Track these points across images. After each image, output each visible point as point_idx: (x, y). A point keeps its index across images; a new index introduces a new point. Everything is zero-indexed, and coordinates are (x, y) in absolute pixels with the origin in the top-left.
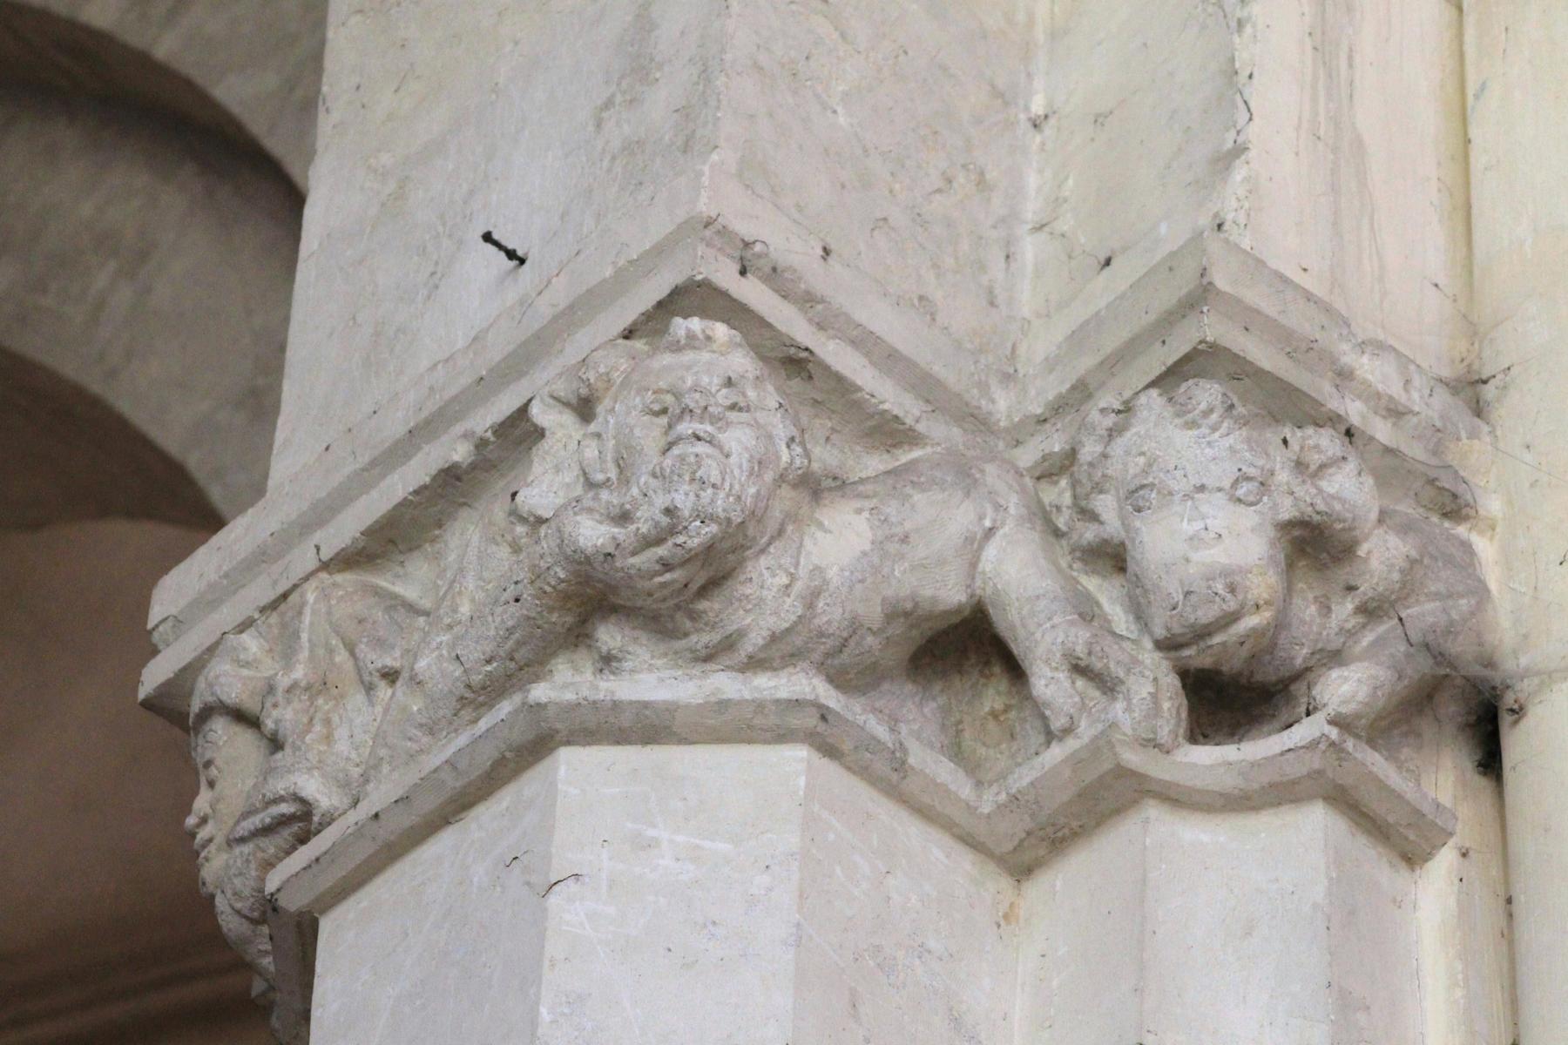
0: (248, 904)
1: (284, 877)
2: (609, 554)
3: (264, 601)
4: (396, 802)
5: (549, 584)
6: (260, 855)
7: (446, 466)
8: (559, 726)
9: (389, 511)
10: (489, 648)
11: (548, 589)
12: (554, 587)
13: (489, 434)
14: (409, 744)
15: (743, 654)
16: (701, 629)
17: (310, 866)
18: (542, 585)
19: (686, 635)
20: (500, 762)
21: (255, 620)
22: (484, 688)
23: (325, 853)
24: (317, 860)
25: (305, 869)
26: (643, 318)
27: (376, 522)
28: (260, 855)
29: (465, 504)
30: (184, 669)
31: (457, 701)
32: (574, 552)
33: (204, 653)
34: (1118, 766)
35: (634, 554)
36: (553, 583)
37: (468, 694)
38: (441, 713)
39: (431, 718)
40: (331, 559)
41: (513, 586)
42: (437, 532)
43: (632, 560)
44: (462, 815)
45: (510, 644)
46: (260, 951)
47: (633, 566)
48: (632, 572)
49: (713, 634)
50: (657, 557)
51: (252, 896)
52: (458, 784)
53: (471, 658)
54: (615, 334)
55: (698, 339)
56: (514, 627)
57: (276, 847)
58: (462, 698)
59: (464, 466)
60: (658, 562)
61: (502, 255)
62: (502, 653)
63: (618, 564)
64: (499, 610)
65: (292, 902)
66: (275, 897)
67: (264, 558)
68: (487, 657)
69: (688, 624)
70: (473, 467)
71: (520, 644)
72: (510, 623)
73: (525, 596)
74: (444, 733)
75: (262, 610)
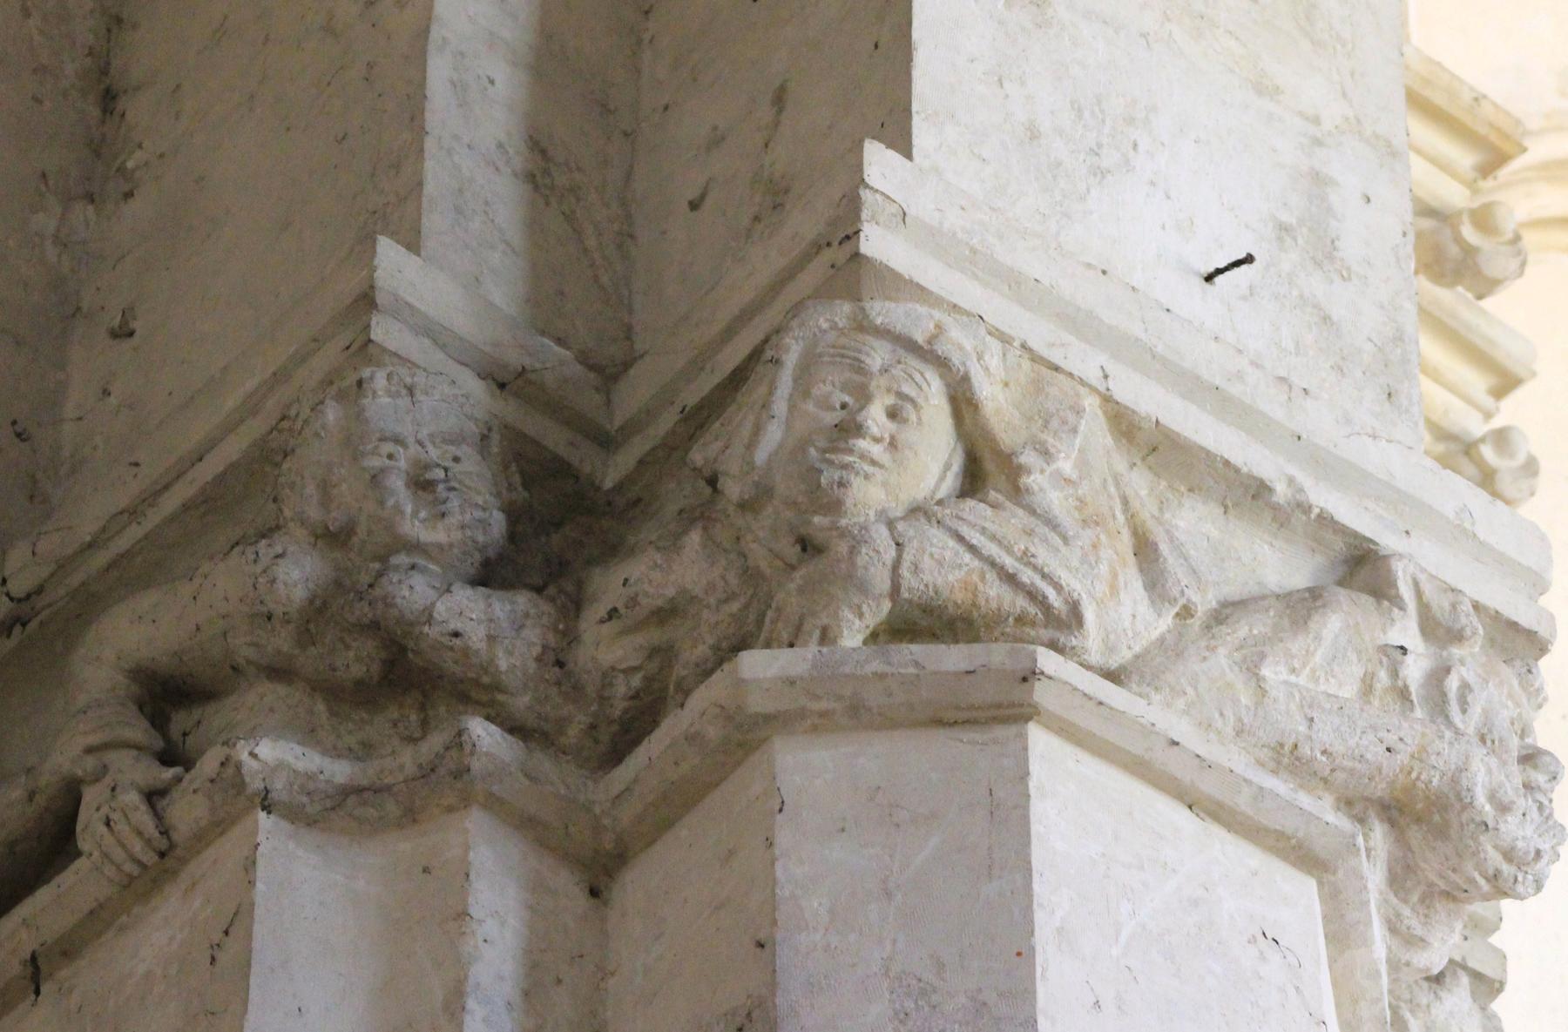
0: (915, 584)
1: (1064, 676)
2: (1487, 826)
3: (1032, 344)
4: (1198, 756)
5: (1420, 773)
6: (975, 578)
7: (1268, 483)
8: (1340, 874)
9: (1195, 443)
10: (1338, 748)
11: (1414, 775)
12: (1418, 778)
13: (1316, 511)
14: (1217, 715)
15: (1407, 957)
16: (1418, 913)
17: (1091, 699)
18: (1416, 768)
19: (1405, 901)
20: (1281, 835)
21: (1011, 344)
22: (1298, 759)
23: (1111, 708)
24: (1101, 703)
25: (1085, 695)
26: (1493, 612)
27: (1178, 435)
28: (975, 578)
29: (1226, 507)
30: (922, 289)
31: (1277, 742)
32: (1469, 790)
33: (949, 303)
34: (777, 859)
35: (1496, 847)
36: (1423, 777)
37: (1287, 749)
38: (1261, 733)
39: (1251, 726)
40: (1117, 403)
41: (1396, 738)
42: (1182, 489)
43: (1489, 848)
44: (1207, 819)
45: (1348, 764)
46: (859, 607)
47: (1485, 852)
48: (1482, 855)
49: (1420, 926)
50: (1499, 867)
51: (926, 586)
52: (1243, 808)
53: (1320, 735)
54: (1471, 596)
55: (1537, 699)
56: (1368, 761)
57: (998, 595)
58: (1282, 745)
59: (1275, 499)
60: (1497, 870)
61: (1222, 265)
62: (1337, 761)
63: (1482, 838)
64: (1371, 736)
65: (1042, 694)
66: (1041, 677)
67: (1013, 285)
68: (1330, 749)
69: (1415, 898)
70: (1276, 508)
71: (1352, 772)
72: (1369, 756)
73: (1399, 757)
74: (1243, 745)
75: (1024, 346)
